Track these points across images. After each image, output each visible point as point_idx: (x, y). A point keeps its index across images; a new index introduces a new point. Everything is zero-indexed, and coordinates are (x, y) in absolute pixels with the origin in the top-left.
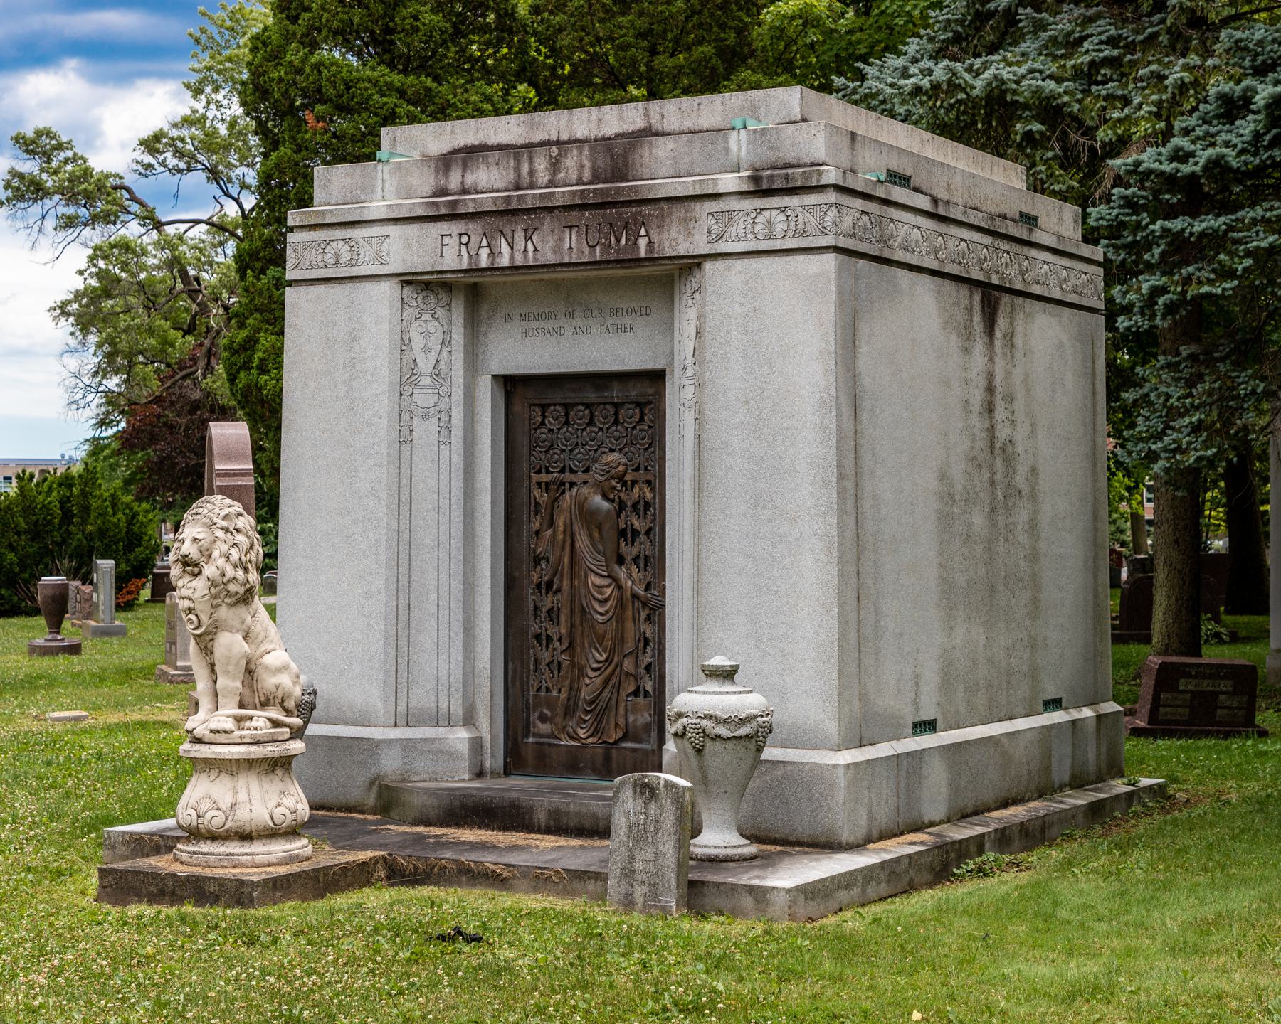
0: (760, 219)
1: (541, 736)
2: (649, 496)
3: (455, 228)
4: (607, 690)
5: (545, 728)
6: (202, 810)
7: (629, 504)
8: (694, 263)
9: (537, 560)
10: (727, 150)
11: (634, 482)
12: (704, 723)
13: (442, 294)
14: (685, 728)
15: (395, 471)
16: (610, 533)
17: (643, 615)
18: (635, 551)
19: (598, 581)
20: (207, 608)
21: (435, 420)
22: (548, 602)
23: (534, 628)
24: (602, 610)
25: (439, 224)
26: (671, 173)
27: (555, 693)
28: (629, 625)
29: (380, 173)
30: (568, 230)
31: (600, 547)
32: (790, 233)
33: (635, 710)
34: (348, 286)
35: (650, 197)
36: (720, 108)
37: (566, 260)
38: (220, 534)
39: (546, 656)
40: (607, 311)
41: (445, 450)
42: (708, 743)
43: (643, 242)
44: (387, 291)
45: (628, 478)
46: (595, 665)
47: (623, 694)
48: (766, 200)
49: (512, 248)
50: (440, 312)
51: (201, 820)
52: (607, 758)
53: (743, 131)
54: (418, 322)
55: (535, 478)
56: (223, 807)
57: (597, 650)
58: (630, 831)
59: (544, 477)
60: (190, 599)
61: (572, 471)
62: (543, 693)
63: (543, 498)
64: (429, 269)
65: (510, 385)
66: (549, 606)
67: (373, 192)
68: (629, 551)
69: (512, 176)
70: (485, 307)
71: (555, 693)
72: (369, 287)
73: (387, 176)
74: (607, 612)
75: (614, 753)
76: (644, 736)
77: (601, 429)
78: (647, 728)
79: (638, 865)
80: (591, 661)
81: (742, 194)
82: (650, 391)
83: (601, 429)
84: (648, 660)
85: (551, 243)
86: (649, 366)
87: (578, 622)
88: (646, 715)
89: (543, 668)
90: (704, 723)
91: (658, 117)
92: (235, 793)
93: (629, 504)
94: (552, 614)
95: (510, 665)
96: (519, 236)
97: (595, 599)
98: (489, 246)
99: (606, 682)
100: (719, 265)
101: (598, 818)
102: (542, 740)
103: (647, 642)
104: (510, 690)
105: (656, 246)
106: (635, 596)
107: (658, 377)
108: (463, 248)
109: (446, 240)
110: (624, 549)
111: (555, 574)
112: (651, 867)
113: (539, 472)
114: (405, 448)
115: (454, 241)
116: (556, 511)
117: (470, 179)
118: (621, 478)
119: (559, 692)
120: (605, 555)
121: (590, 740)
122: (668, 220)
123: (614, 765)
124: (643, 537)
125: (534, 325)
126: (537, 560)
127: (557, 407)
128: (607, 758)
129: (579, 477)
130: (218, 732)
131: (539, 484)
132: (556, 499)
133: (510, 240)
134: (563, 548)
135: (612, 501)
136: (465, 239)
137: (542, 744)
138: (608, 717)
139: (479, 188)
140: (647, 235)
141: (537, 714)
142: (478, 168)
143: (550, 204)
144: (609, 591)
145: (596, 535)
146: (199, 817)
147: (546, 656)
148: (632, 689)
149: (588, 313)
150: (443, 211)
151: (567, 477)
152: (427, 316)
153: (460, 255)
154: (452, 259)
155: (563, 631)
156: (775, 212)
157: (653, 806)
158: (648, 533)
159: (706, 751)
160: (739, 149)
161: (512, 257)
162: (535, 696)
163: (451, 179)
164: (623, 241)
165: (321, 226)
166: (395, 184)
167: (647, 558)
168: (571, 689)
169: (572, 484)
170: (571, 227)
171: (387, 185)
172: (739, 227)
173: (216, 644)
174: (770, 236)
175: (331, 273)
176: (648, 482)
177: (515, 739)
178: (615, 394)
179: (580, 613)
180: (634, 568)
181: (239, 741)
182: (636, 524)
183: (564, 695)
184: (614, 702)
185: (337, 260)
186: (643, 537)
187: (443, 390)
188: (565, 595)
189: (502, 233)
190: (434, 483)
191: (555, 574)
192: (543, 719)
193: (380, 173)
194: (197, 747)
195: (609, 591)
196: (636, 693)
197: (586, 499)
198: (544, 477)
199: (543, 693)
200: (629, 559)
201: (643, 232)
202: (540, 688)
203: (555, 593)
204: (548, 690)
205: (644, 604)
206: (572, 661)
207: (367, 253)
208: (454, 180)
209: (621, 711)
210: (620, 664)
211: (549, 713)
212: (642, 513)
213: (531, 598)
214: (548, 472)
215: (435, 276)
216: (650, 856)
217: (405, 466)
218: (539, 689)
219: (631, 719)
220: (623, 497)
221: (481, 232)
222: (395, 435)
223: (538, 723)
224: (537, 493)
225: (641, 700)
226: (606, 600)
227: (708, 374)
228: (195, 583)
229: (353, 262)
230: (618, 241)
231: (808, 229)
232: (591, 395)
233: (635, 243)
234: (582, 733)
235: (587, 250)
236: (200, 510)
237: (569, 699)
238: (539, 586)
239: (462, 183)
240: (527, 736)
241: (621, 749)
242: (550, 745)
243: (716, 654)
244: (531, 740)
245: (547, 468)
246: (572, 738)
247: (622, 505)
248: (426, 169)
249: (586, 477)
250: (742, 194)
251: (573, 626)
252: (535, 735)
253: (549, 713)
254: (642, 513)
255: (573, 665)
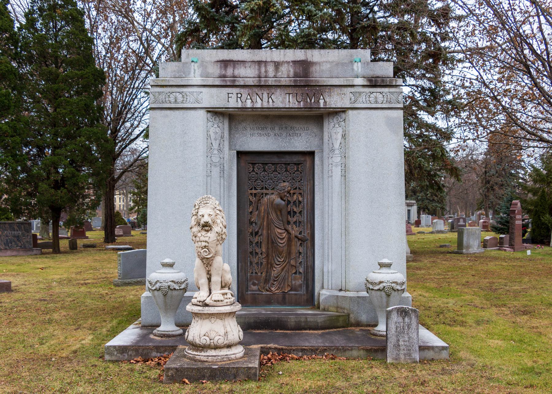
0: (372, 96)
1: (253, 291)
2: (301, 199)
3: (235, 90)
4: (283, 273)
5: (255, 288)
6: (212, 337)
7: (292, 202)
8: (344, 110)
9: (251, 223)
10: (353, 69)
11: (294, 194)
12: (393, 285)
13: (221, 118)
14: (384, 287)
15: (205, 187)
16: (284, 212)
17: (299, 244)
18: (294, 220)
19: (280, 231)
20: (214, 246)
21: (219, 168)
22: (256, 239)
23: (250, 250)
24: (282, 242)
25: (227, 89)
26: (329, 76)
27: (259, 274)
28: (293, 247)
29: (193, 67)
30: (288, 95)
31: (281, 218)
32: (385, 102)
33: (295, 279)
34: (182, 112)
35: (325, 84)
36: (337, 55)
37: (287, 106)
38: (218, 212)
39: (255, 260)
40: (290, 128)
41: (222, 181)
42: (393, 292)
43: (322, 102)
44: (202, 113)
45: (292, 192)
46: (278, 263)
47: (290, 274)
48: (374, 89)
49: (262, 100)
50: (220, 125)
51: (212, 341)
52: (284, 298)
53: (359, 63)
54: (213, 128)
55: (250, 192)
56: (222, 334)
57: (279, 257)
58: (397, 329)
59: (254, 191)
60: (206, 242)
61: (266, 189)
62: (254, 274)
63: (253, 199)
64: (222, 106)
65: (240, 154)
66: (256, 241)
67: (189, 74)
68: (292, 220)
69: (257, 72)
70: (234, 124)
71: (259, 274)
72: (193, 112)
73: (196, 68)
74: (284, 243)
75: (287, 296)
76: (299, 289)
77: (279, 173)
78: (300, 286)
79: (401, 343)
80: (276, 262)
81: (364, 86)
82: (302, 159)
83: (279, 173)
84: (301, 260)
85: (281, 99)
86: (309, 150)
87: (270, 246)
88: (300, 281)
89: (254, 265)
90: (393, 285)
91: (310, 56)
92: (225, 327)
93: (292, 202)
94: (259, 244)
95: (240, 264)
96: (265, 96)
97: (279, 238)
98: (251, 99)
99: (283, 269)
100: (355, 112)
101: (318, 323)
102: (254, 292)
103: (300, 253)
104: (240, 274)
105: (328, 103)
106: (296, 237)
107: (312, 154)
108: (239, 99)
109: (230, 95)
110: (290, 219)
111: (260, 228)
112: (407, 343)
113: (251, 189)
114: (209, 178)
115: (234, 96)
116: (259, 205)
117: (236, 72)
118: (289, 192)
119: (261, 273)
120: (282, 221)
121: (276, 291)
122: (333, 94)
123: (287, 300)
124: (298, 214)
125: (256, 132)
126: (251, 223)
127: (260, 165)
128: (284, 298)
129: (270, 191)
130: (219, 301)
131: (251, 194)
132: (260, 200)
133: (261, 97)
134: (263, 219)
135: (284, 201)
136: (239, 96)
137: (255, 294)
138: (284, 283)
139: (241, 76)
140: (324, 99)
141: (251, 283)
142: (241, 68)
143: (279, 84)
144: (284, 235)
145: (279, 213)
146: (210, 340)
147: (255, 260)
148: (294, 271)
149: (281, 128)
150: (228, 84)
151: (264, 191)
152: (216, 126)
153: (268, 101)
154: (233, 103)
155: (264, 250)
156: (378, 94)
157: (406, 319)
158: (300, 212)
159: (392, 296)
160: (358, 69)
161: (262, 104)
162: (251, 276)
163: (228, 71)
164: (313, 101)
165: (166, 86)
166: (200, 71)
167: (300, 222)
168: (267, 272)
169: (266, 194)
170: (289, 94)
171: (196, 71)
172: (363, 98)
173: (214, 261)
174: (376, 102)
175: (173, 106)
176: (300, 194)
177: (242, 293)
178: (288, 159)
179: (272, 242)
180: (294, 226)
181: (226, 304)
182: (295, 210)
183: (264, 275)
184: (287, 277)
185: (176, 100)
186: (298, 214)
187: (221, 156)
188: (265, 236)
189: (257, 94)
190: (219, 192)
191: (260, 228)
192: (254, 284)
193: (193, 67)
194: (207, 308)
195: (284, 235)
196: (295, 273)
197: (274, 200)
198: (254, 191)
199: (254, 274)
200: (292, 222)
201: (322, 97)
202: (252, 273)
203: (259, 236)
204: (256, 273)
205: (299, 239)
206: (268, 262)
207: (191, 99)
208: (230, 72)
209: (290, 280)
210: (289, 262)
211: (257, 282)
212: (297, 205)
213: (248, 238)
214: (255, 189)
215: (224, 110)
216: (407, 339)
217: (209, 186)
218: (252, 273)
219: (294, 282)
220: (289, 199)
221: (247, 93)
222: (205, 173)
223: (252, 286)
224: (251, 198)
225: (298, 275)
226: (283, 238)
227: (351, 153)
228: (209, 234)
229: (184, 102)
230: (311, 101)
231: (392, 100)
232: (276, 160)
233: (318, 101)
234: (273, 289)
235: (297, 103)
236: (208, 202)
237: (266, 276)
238: (252, 234)
239: (233, 73)
240: (247, 291)
241: (289, 294)
242: (258, 294)
243: (384, 258)
244: (249, 292)
245: (255, 188)
246: (267, 291)
247: (289, 202)
248: (215, 66)
249: (272, 191)
250: (364, 86)
251: (268, 248)
252: (250, 291)
253: (257, 282)
254: (297, 205)
255: (268, 263)
